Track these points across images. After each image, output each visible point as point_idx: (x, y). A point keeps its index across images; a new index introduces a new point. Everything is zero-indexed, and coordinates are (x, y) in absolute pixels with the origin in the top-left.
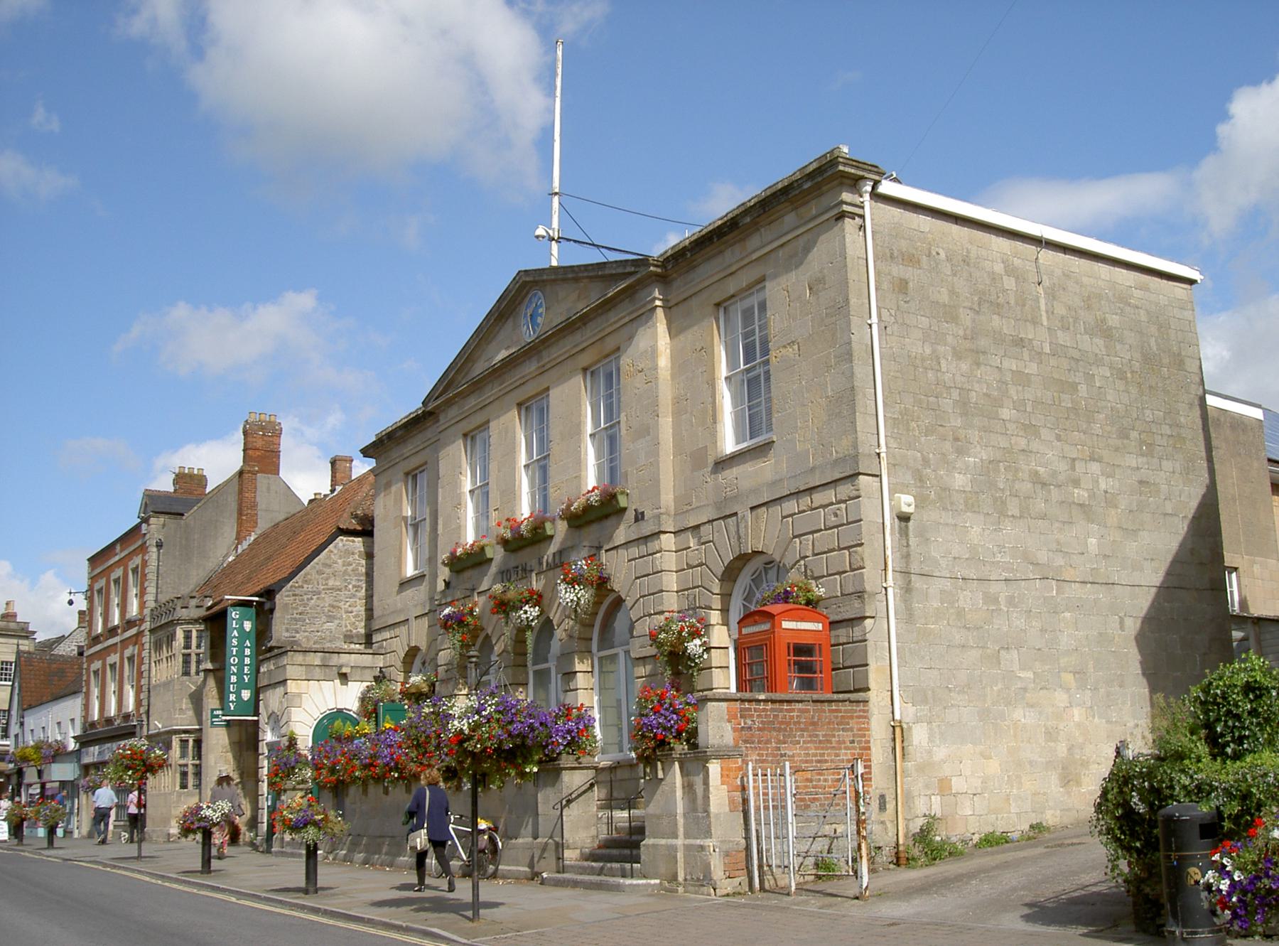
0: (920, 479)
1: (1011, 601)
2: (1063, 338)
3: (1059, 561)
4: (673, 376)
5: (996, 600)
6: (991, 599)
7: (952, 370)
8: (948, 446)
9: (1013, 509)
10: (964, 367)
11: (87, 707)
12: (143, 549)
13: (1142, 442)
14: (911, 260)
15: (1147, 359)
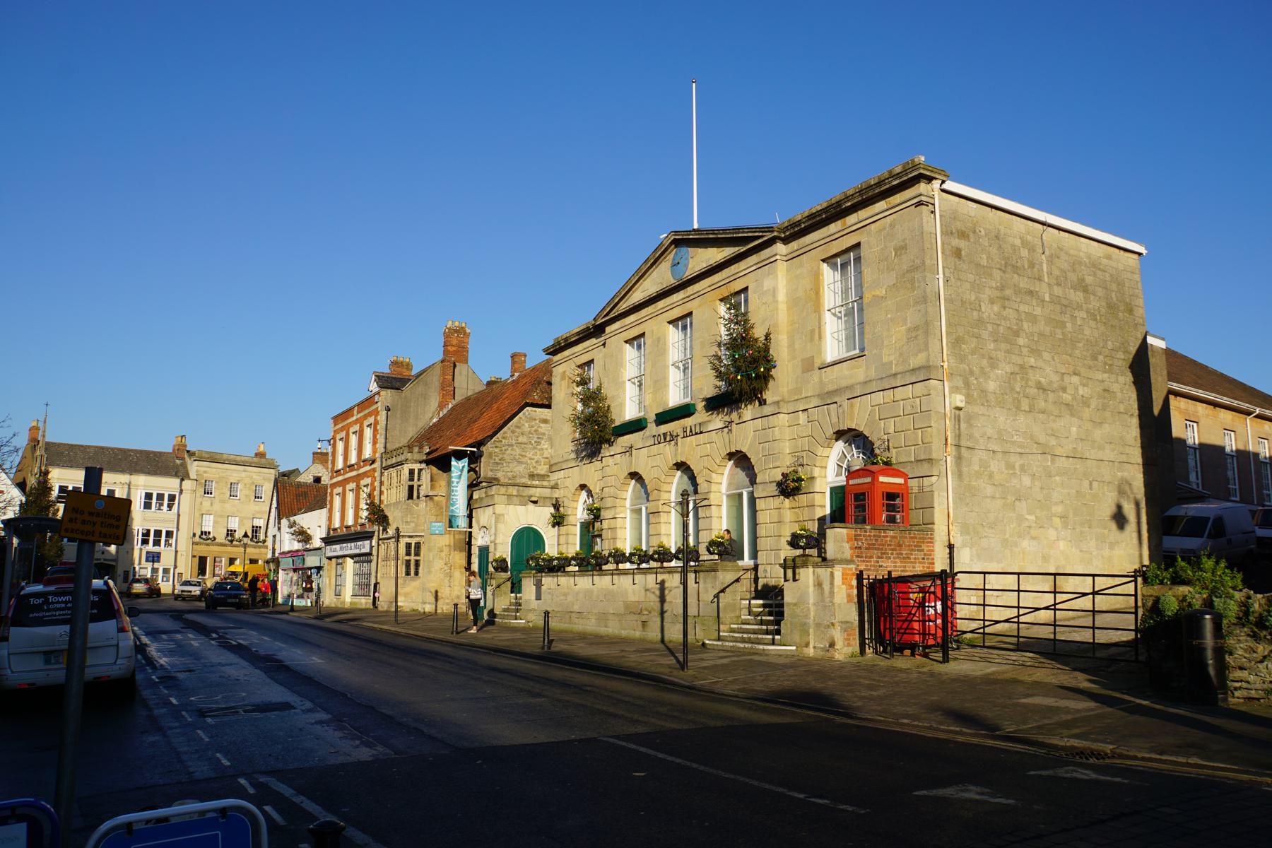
0: (967, 384)
1: (1022, 467)
2: (1058, 291)
3: (1053, 442)
4: (789, 309)
5: (1013, 467)
6: (1010, 466)
7: (989, 310)
8: (985, 362)
9: (1025, 405)
10: (996, 308)
11: (330, 519)
12: (376, 413)
13: (1106, 363)
14: (963, 235)
15: (1110, 306)
